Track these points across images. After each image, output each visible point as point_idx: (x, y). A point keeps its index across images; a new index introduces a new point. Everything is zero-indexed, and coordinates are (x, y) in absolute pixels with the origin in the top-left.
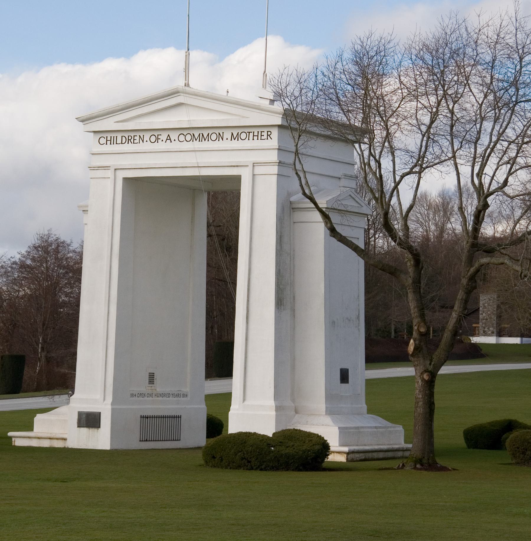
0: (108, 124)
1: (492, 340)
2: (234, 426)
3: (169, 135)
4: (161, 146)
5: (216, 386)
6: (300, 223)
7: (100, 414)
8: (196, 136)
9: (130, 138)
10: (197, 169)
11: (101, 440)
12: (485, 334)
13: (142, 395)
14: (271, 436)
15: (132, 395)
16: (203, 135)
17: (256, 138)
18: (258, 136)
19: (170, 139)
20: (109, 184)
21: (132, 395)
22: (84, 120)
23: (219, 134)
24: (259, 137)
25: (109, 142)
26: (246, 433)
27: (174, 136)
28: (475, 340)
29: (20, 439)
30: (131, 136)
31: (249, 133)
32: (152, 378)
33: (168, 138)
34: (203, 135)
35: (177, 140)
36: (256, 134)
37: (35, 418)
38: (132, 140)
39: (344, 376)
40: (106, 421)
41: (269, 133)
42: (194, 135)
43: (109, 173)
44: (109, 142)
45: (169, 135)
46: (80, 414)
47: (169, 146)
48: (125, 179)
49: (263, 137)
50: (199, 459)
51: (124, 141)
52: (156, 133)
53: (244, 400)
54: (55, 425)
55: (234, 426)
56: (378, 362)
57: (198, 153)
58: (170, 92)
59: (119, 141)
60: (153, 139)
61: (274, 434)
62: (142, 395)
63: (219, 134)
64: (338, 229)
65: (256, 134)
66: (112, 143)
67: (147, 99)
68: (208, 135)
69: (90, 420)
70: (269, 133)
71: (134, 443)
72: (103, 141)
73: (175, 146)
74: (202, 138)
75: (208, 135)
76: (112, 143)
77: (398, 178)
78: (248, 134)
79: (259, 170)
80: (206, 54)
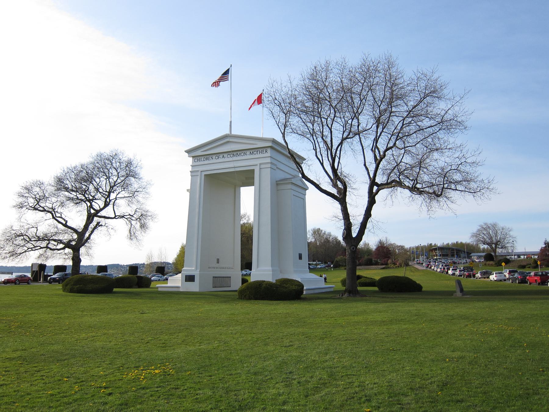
0: (199, 153)
4: (221, 160)
7: (194, 276)
11: (194, 287)
15: (209, 268)
20: (199, 178)
21: (209, 268)
22: (188, 152)
26: (260, 281)
27: (225, 155)
30: (207, 157)
32: (218, 260)
39: (300, 257)
40: (197, 279)
47: (223, 160)
53: (258, 267)
60: (217, 158)
64: (294, 166)
69: (190, 278)
72: (196, 160)
73: (226, 159)
77: (330, 126)
79: (262, 166)
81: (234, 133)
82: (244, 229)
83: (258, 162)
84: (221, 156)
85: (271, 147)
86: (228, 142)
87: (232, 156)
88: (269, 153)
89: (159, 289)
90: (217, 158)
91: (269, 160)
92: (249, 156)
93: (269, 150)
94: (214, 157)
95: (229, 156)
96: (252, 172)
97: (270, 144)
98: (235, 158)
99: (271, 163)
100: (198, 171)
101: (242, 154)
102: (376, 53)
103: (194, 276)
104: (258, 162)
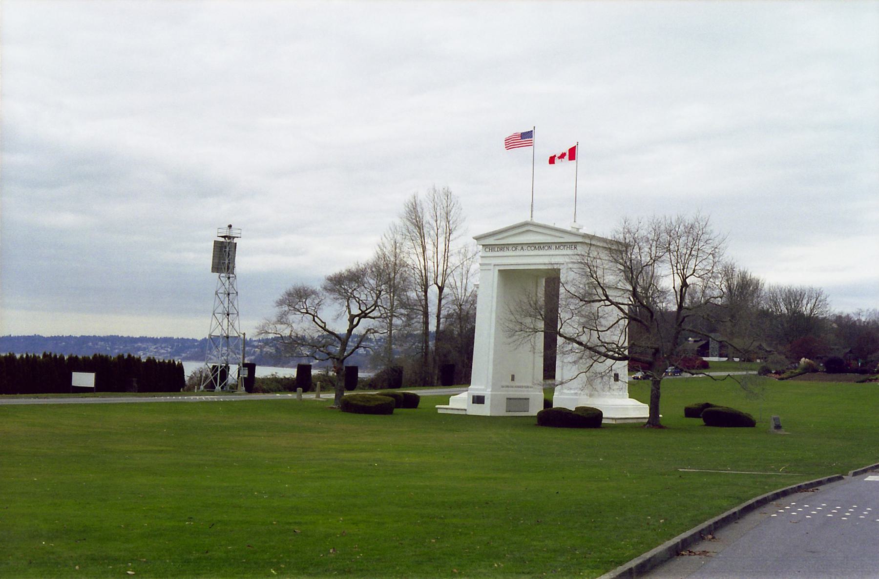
1: (716, 359)
2: (555, 405)
5: (550, 382)
11: (484, 410)
12: (713, 356)
13: (508, 387)
14: (574, 409)
15: (503, 387)
21: (503, 387)
22: (477, 239)
28: (705, 359)
29: (441, 409)
30: (502, 247)
43: (492, 267)
46: (474, 397)
48: (499, 271)
50: (536, 421)
52: (515, 246)
54: (459, 401)
55: (555, 405)
56: (21, 393)
62: (508, 387)
64: (649, 315)
69: (479, 400)
71: (502, 412)
73: (526, 253)
80: (662, 305)
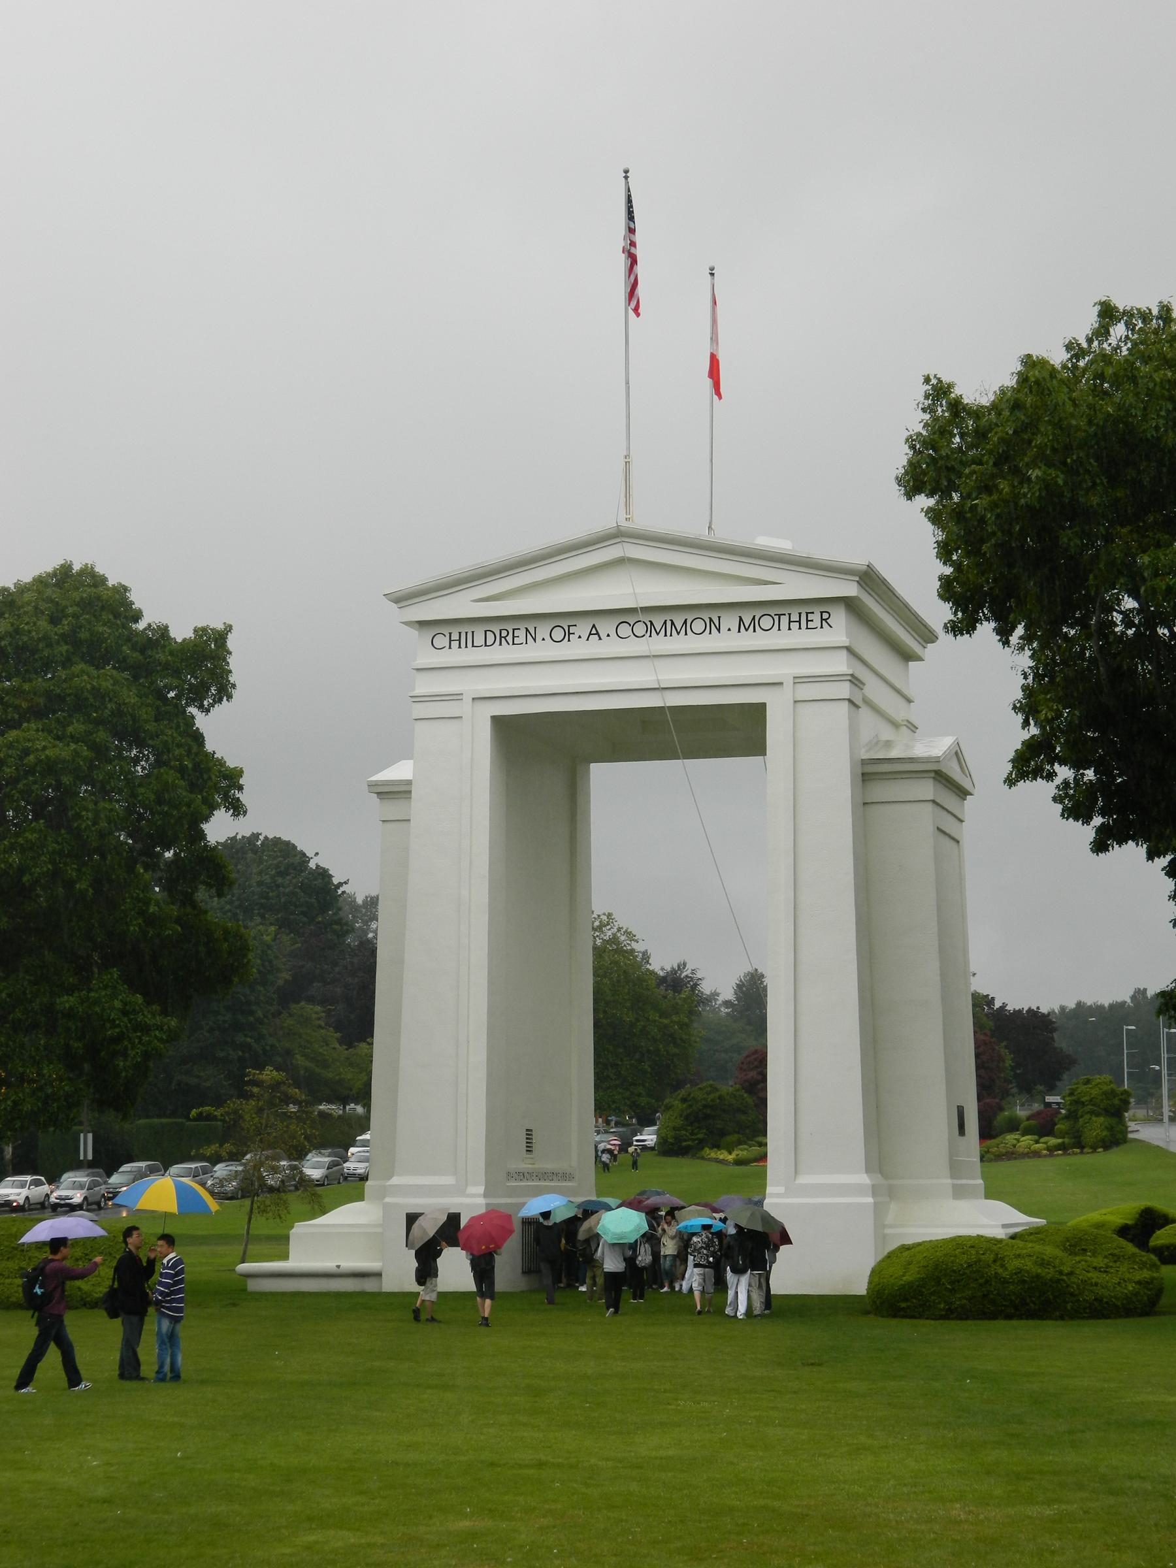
3: (594, 626)
4: (578, 648)
6: (887, 807)
7: (765, 704)
8: (679, 625)
9: (504, 633)
10: (657, 694)
16: (673, 623)
17: (795, 626)
18: (799, 622)
19: (597, 633)
22: (401, 599)
23: (711, 620)
24: (803, 622)
25: (455, 644)
27: (729, 621)
30: (505, 628)
31: (779, 615)
33: (594, 631)
34: (673, 623)
35: (613, 634)
36: (795, 617)
37: (209, 747)
38: (510, 639)
41: (825, 616)
42: (652, 623)
44: (455, 644)
45: (594, 626)
47: (594, 648)
49: (810, 625)
51: (490, 640)
52: (564, 622)
57: (657, 662)
58: (488, 569)
59: (479, 640)
61: (184, 640)
63: (711, 620)
65: (795, 617)
66: (463, 645)
67: (548, 550)
68: (754, 618)
70: (825, 616)
74: (670, 628)
75: (754, 618)
76: (463, 645)
78: (776, 618)
81: (643, 520)
82: (1035, 374)
83: (783, 669)
84: (583, 628)
85: (849, 604)
86: (621, 561)
87: (640, 629)
88: (840, 629)
89: (253, 1286)
90: (558, 634)
91: (840, 664)
92: (729, 638)
93: (839, 617)
94: (543, 631)
95: (625, 630)
96: (757, 712)
97: (850, 589)
98: (660, 644)
99: (855, 681)
100: (457, 697)
101: (698, 626)
102: (1143, 1204)
103: (765, 704)
104: (783, 669)
